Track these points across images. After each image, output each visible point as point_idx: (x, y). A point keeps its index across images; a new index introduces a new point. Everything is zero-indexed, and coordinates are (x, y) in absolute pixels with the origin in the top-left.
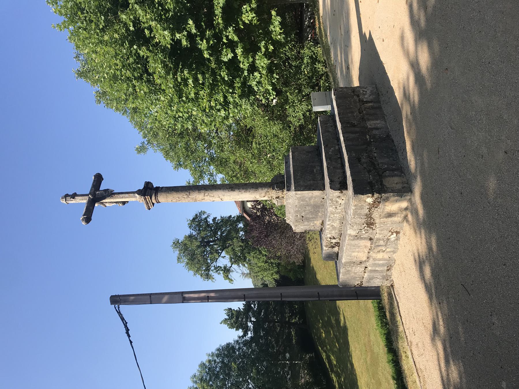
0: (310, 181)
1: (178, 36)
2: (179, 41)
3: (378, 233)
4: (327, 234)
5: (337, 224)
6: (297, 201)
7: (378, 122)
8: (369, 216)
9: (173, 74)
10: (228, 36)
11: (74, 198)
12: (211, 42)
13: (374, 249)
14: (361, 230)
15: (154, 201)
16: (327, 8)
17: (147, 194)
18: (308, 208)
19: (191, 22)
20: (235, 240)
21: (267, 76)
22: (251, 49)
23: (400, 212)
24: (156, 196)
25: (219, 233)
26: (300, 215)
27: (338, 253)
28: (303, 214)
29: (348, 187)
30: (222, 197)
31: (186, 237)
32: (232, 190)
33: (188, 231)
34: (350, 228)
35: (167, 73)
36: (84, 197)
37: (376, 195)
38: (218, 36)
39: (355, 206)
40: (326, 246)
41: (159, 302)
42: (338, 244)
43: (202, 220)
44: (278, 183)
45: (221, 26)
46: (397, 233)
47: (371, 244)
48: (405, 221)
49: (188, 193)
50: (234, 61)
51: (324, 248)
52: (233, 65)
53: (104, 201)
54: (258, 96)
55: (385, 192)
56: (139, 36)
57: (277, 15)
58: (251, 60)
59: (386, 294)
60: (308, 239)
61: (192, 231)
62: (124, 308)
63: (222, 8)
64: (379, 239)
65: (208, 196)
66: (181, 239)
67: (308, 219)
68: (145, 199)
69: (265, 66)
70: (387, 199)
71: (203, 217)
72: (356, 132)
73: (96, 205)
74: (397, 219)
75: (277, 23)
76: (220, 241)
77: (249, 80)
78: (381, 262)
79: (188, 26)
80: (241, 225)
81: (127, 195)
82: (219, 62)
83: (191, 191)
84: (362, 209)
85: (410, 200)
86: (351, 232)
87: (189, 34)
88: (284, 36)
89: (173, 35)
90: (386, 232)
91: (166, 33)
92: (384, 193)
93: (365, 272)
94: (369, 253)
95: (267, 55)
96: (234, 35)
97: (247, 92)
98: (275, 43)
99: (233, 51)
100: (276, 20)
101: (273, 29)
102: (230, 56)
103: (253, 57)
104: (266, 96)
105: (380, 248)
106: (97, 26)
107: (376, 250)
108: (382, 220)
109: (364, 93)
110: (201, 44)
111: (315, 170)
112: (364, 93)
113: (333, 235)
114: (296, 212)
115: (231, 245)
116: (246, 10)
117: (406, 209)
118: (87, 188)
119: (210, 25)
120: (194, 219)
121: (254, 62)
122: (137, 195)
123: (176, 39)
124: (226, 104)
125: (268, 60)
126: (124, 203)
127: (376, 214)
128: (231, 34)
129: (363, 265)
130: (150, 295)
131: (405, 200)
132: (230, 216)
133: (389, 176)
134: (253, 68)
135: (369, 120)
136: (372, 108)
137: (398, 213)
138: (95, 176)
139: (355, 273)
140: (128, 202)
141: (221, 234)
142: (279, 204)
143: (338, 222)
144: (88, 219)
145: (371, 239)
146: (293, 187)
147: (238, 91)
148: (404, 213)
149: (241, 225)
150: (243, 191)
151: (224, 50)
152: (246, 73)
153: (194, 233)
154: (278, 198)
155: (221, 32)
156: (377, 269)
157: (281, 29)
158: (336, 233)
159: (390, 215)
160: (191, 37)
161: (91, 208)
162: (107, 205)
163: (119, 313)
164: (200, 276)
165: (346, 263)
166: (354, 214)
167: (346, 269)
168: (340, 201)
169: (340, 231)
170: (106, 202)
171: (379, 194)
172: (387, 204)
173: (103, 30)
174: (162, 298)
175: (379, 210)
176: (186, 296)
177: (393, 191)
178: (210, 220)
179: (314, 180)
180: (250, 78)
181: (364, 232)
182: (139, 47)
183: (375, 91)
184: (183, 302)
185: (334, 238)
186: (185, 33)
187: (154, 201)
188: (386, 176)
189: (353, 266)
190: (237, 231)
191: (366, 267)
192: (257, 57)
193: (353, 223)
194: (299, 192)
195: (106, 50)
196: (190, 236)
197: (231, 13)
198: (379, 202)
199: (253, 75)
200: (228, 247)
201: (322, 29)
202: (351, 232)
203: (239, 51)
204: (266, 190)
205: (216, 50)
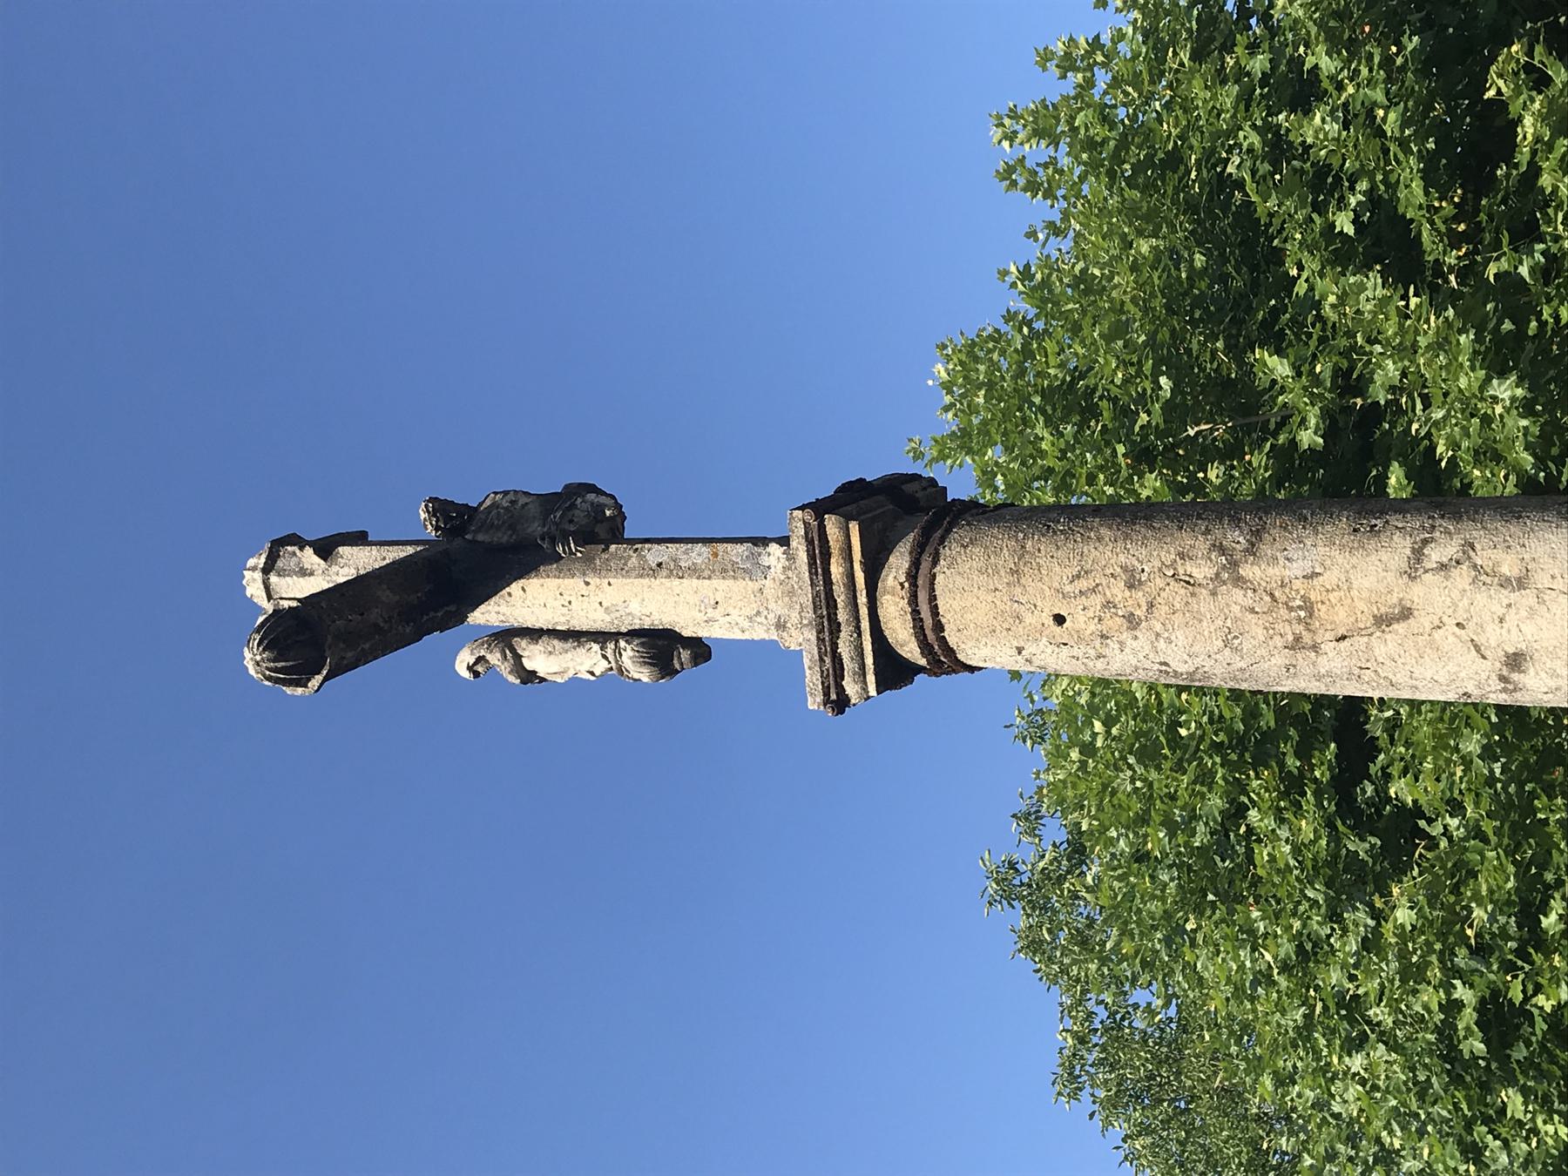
49: (1236, 538)
65: (1462, 576)
126: (663, 647)
140: (700, 650)
170: (535, 634)
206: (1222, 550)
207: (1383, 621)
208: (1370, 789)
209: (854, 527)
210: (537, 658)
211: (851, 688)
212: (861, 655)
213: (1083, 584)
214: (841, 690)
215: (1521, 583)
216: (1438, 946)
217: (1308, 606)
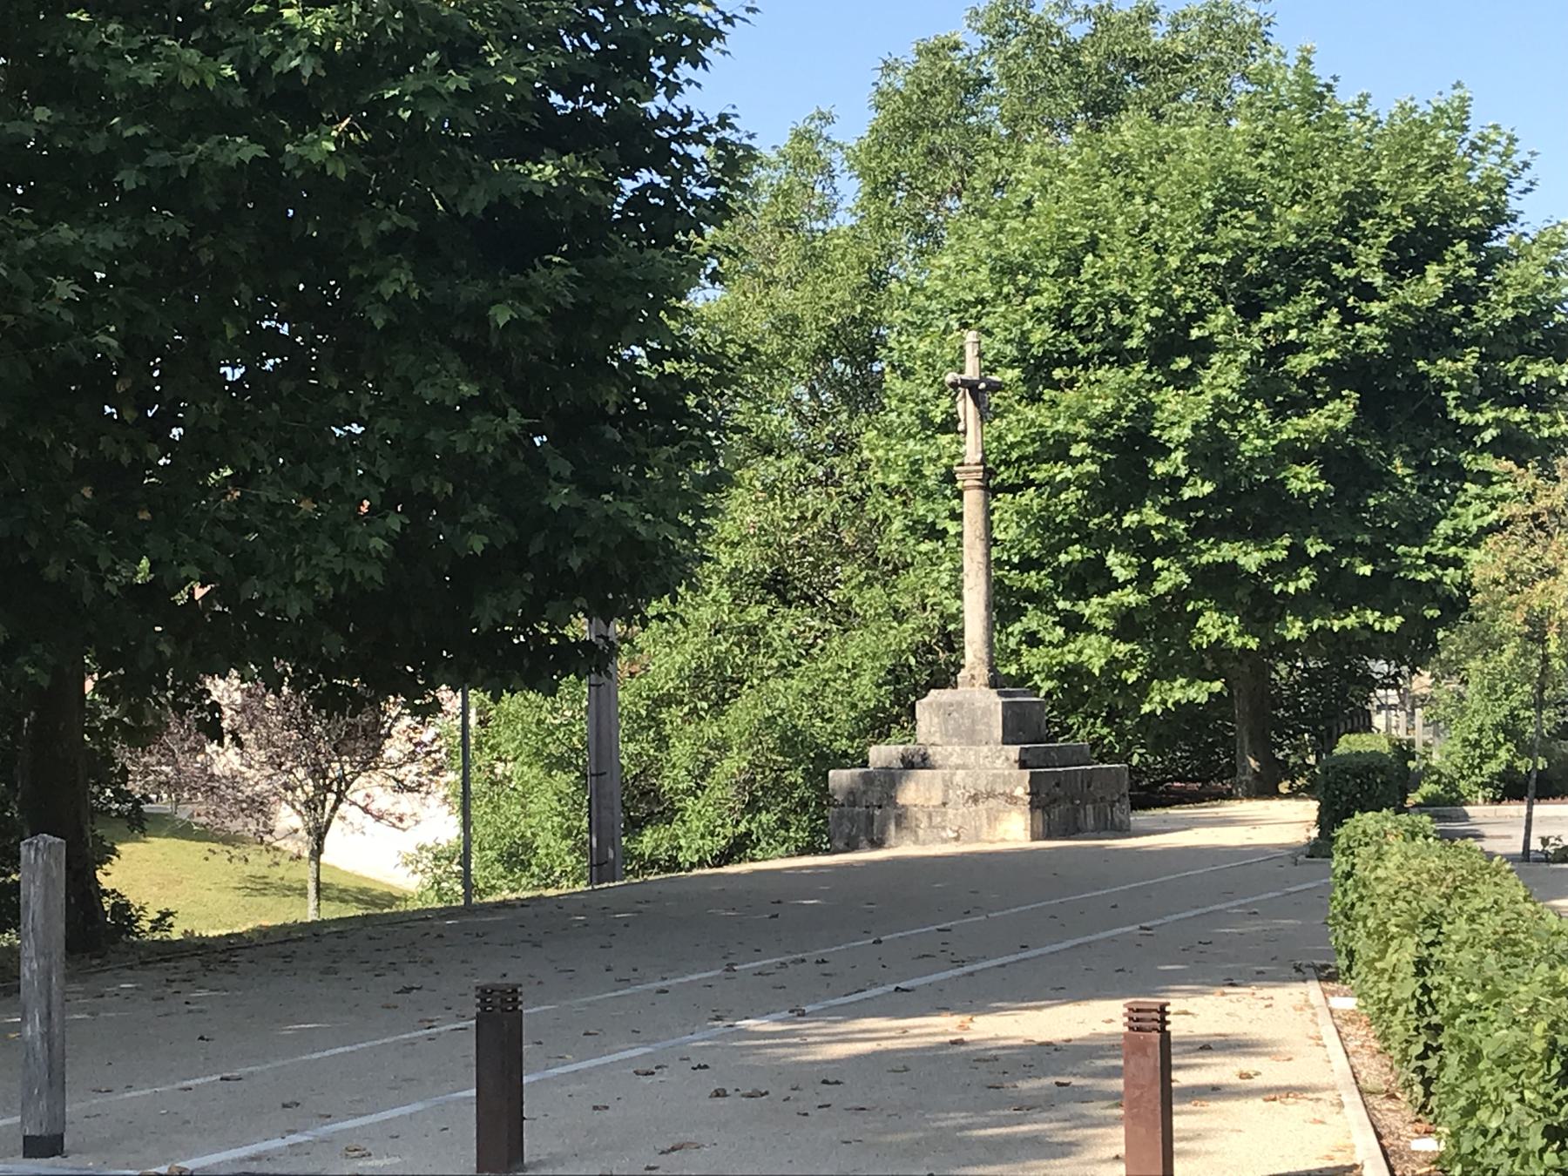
1: (1179, 455)
8: (991, 795)
12: (1157, 537)
18: (967, 722)
19: (1208, 488)
21: (1060, 664)
22: (1126, 625)
24: (980, 487)
35: (1092, 423)
38: (1170, 548)
52: (1091, 578)
56: (1177, 349)
58: (1101, 624)
69: (1084, 658)
75: (1192, 693)
87: (1182, 482)
90: (959, 821)
96: (1170, 584)
100: (1199, 693)
101: (1177, 684)
102: (1121, 574)
103: (1105, 632)
119: (1199, 530)
125: (1101, 669)
128: (1170, 576)
134: (1074, 625)
145: (944, 804)
151: (1134, 560)
152: (1061, 604)
154: (973, 677)
157: (1177, 703)
180: (1048, 613)
186: (1183, 472)
192: (1105, 640)
197: (1220, 583)
199: (1055, 624)
203: (1131, 597)
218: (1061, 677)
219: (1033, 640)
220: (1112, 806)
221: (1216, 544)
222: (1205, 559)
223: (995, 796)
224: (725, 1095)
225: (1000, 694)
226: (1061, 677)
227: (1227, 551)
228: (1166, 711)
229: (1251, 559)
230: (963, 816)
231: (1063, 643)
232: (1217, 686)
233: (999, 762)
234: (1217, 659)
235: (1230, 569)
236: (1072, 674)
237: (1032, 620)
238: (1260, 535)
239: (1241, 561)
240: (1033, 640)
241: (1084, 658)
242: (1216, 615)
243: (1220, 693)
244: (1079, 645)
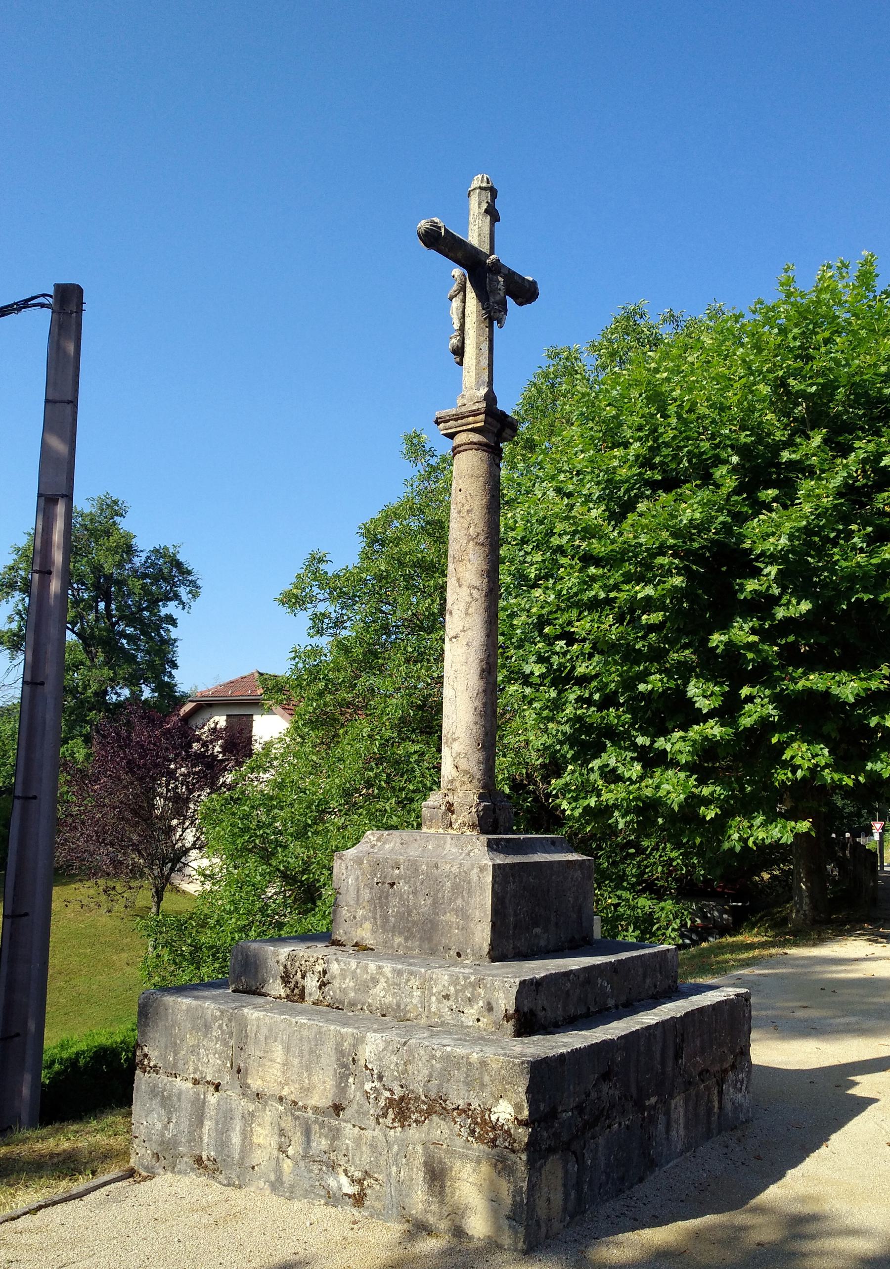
0: (516, 915)
1: (772, 570)
2: (756, 573)
3: (363, 1137)
4: (341, 966)
5: (380, 994)
6: (455, 869)
7: (682, 1132)
8: (437, 1107)
9: (675, 545)
10: (752, 702)
11: (487, 211)
12: (750, 656)
13: (297, 1118)
14: (380, 1078)
15: (461, 439)
16: (834, 968)
17: (490, 420)
19: (805, 606)
20: (107, 672)
22: (706, 762)
23: (446, 1210)
24: (480, 446)
25: (129, 630)
26: (399, 877)
27: (264, 995)
28: (403, 887)
29: (526, 1040)
30: (463, 640)
31: (129, 536)
32: (483, 671)
33: (145, 543)
34: (388, 1043)
36: (487, 240)
37: (523, 1134)
38: (762, 674)
39: (483, 1063)
40: (292, 958)
41: (49, 426)
42: (297, 995)
43: (174, 585)
44: (494, 811)
45: (788, 686)
46: (359, 1200)
47: (316, 1109)
48: (406, 1226)
49: (481, 539)
50: (690, 715)
51: (284, 951)
52: (676, 711)
53: (471, 295)
54: (570, 767)
55: (531, 1162)
56: (765, 473)
57: (797, 836)
58: (683, 759)
59: (66, 1145)
60: (111, 884)
61: (144, 555)
62: (39, 321)
63: (827, 694)
64: (335, 1134)
65: (469, 599)
66: (125, 524)
67: (380, 902)
68: (474, 413)
69: (661, 793)
70: (501, 1166)
71: (183, 591)
72: (663, 1063)
73: (457, 271)
74: (419, 1199)
76: (106, 630)
77: (620, 748)
78: (236, 1139)
79: (794, 601)
80: (147, 693)
81: (485, 363)
82: (684, 671)
83: (487, 548)
84: (467, 1084)
85: (493, 1246)
86: (373, 1046)
87: (775, 601)
88: (738, 849)
89: (772, 559)
90: (365, 1158)
91: (784, 541)
92: (528, 1160)
93: (196, 1082)
94: (281, 1099)
95: (693, 802)
96: (755, 717)
97: (588, 741)
98: (720, 825)
99: (711, 714)
100: (782, 832)
102: (704, 705)
104: (570, 791)
105: (297, 1138)
106: (795, 373)
107: (288, 1123)
108: (420, 1149)
109: (739, 1085)
110: (741, 628)
111: (537, 930)
112: (739, 1085)
113: (336, 983)
114: (414, 866)
115: (92, 660)
116: (817, 755)
117: (459, 1232)
118: (512, 256)
119: (791, 656)
120: (178, 565)
121: (674, 764)
122: (484, 391)
123: (762, 565)
124: (561, 679)
125: (680, 806)
126: (459, 351)
127: (439, 1129)
128: (758, 708)
129: (226, 1079)
130: (73, 402)
131: (498, 1229)
132: (174, 666)
133: (566, 1172)
134: (653, 760)
135: (686, 1102)
136: (710, 1111)
137: (442, 1202)
138: (534, 283)
139: (194, 1050)
140: (461, 363)
141: (126, 636)
142: (425, 812)
143: (389, 999)
144: (433, 239)
145: (337, 1109)
146: (501, 859)
147: (592, 714)
148: (443, 1225)
149: (147, 693)
150: (478, 704)
151: (717, 689)
152: (641, 740)
153: (137, 561)
154: (450, 808)
155: (771, 683)
156: (208, 1124)
158: (344, 991)
159: (437, 1176)
160: (762, 605)
161: (459, 255)
162: (456, 303)
163: (25, 304)
164: (11, 563)
165: (243, 1024)
166: (447, 1058)
167: (215, 1019)
168: (472, 1012)
169: (352, 1004)
170: (464, 301)
171: (528, 1144)
172: (485, 1168)
173: (782, 383)
174: (61, 436)
175: (459, 1141)
176: (60, 509)
177: (532, 1187)
178: (170, 608)
179: (515, 927)
180: (626, 749)
181: (368, 1086)
182: (735, 470)
183: (742, 1117)
184: (40, 495)
185: (323, 985)
186: (776, 591)
187: (461, 439)
188: (566, 1162)
189: (226, 1044)
190: (133, 681)
191: (217, 1087)
192: (682, 775)
193: (410, 1052)
194: (490, 879)
195: (736, 385)
196: (129, 550)
197: (810, 715)
198: (494, 1141)
200: (88, 653)
201: (750, 954)
202: (373, 1046)
203: (714, 730)
204: (478, 775)
205: (729, 668)
206: (477, 536)
207: (458, 580)
208: (648, 493)
209: (482, 424)
210: (456, 303)
211: (442, 425)
212: (450, 428)
213: (468, 497)
214: (441, 422)
215: (467, 614)
216: (579, 529)
217: (462, 560)
218: (638, 811)
219: (612, 776)
220: (720, 1083)
221: (805, 674)
222: (801, 685)
223: (444, 1113)
224: (489, 1004)
225: (492, 846)
226: (638, 811)
227: (815, 681)
228: (746, 848)
229: (848, 688)
230: (373, 1147)
231: (641, 778)
232: (804, 826)
233: (472, 1012)
234: (807, 796)
235: (823, 701)
236: (648, 809)
237: (610, 758)
238: (852, 662)
239: (835, 690)
240: (612, 776)
241: (661, 793)
242: (805, 746)
243: (807, 833)
244: (656, 780)
